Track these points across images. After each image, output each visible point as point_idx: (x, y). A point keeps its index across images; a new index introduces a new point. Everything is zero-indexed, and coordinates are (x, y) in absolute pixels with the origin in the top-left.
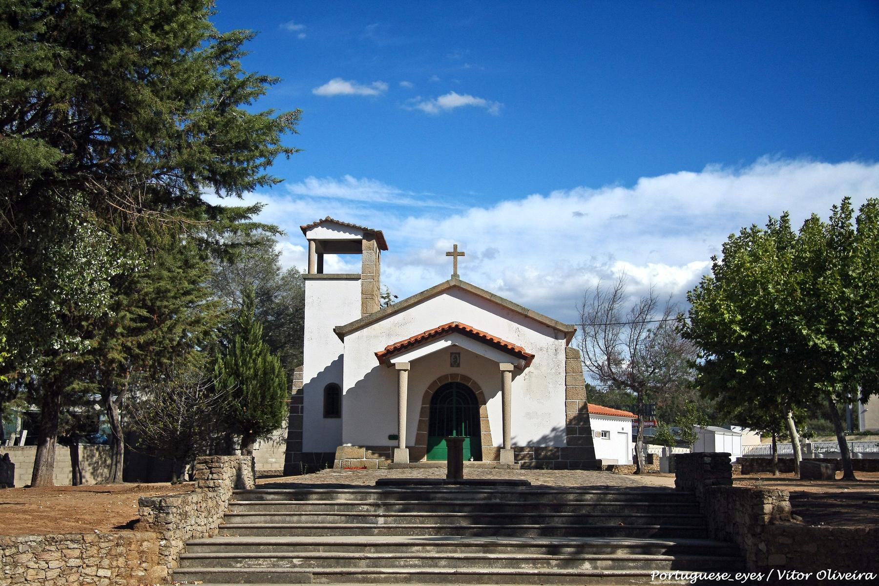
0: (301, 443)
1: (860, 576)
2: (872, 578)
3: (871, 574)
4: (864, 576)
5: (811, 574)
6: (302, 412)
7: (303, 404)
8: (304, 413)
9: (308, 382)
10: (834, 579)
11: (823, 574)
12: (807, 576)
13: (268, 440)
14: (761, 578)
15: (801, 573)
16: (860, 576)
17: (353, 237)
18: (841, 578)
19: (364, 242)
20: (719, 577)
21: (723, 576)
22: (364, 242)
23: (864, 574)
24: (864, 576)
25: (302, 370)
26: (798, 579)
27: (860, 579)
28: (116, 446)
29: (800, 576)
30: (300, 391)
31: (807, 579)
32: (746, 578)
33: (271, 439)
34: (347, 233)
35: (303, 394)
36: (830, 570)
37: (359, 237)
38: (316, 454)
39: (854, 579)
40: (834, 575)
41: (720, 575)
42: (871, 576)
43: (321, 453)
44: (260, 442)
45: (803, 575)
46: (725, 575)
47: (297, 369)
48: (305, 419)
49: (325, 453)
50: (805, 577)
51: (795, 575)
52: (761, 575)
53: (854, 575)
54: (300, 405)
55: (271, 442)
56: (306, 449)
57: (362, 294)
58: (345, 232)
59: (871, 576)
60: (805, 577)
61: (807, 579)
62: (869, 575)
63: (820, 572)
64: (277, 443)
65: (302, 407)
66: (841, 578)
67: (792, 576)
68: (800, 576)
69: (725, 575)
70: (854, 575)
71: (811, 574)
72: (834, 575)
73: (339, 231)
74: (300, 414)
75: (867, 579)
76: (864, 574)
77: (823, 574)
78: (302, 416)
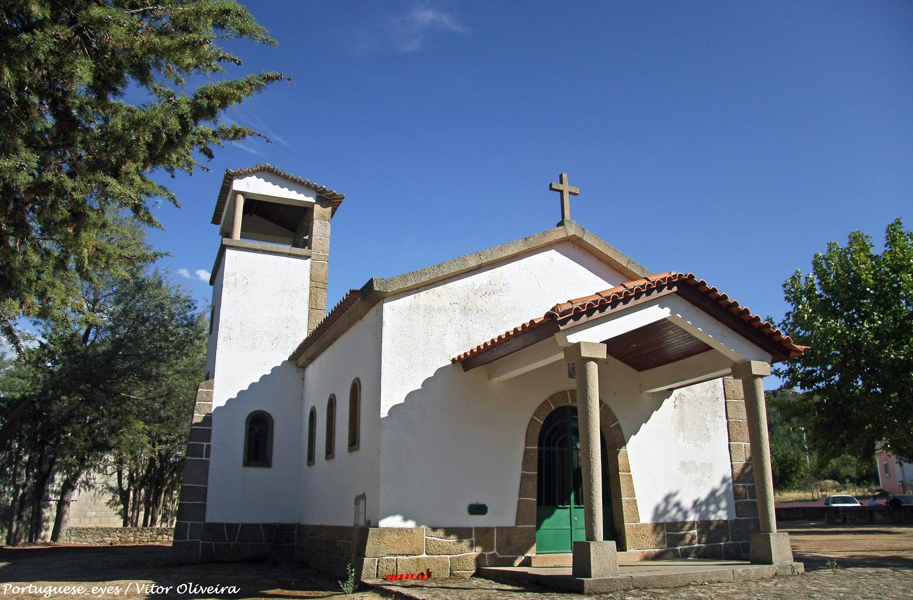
0: (204, 506)
1: (223, 590)
2: (235, 592)
3: (235, 588)
4: (227, 590)
5: (172, 587)
6: (208, 456)
7: (209, 441)
8: (211, 456)
9: (223, 404)
10: (195, 593)
11: (184, 587)
12: (167, 590)
13: (89, 488)
14: (118, 591)
15: (161, 587)
16: (223, 590)
17: (301, 197)
18: (203, 592)
19: (317, 208)
20: (75, 591)
21: (78, 590)
22: (317, 208)
23: (227, 587)
24: (227, 590)
25: (211, 387)
26: (158, 593)
27: (222, 593)
28: (522, 588)
29: (160, 590)
30: (208, 419)
31: (166, 593)
32: (103, 592)
33: (93, 487)
34: (286, 189)
35: (211, 426)
36: (191, 584)
37: (311, 199)
38: (230, 526)
39: (216, 593)
40: (195, 589)
41: (76, 589)
42: (234, 590)
43: (237, 525)
44: (80, 491)
45: (163, 589)
46: (81, 588)
47: (203, 383)
48: (211, 467)
49: (243, 525)
50: (165, 590)
51: (155, 589)
52: (119, 589)
53: (217, 589)
54: (205, 444)
55: (93, 491)
56: (212, 517)
57: (311, 280)
58: (290, 190)
59: (234, 590)
60: (165, 590)
61: (166, 593)
62: (232, 589)
63: (181, 586)
64: (100, 492)
65: (209, 447)
66: (203, 592)
67: (152, 590)
68: (160, 590)
69: (81, 588)
70: (217, 589)
71: (172, 587)
72: (195, 589)
73: (282, 187)
74: (204, 458)
75: (229, 592)
76: (227, 587)
77: (184, 587)
78: (208, 461)
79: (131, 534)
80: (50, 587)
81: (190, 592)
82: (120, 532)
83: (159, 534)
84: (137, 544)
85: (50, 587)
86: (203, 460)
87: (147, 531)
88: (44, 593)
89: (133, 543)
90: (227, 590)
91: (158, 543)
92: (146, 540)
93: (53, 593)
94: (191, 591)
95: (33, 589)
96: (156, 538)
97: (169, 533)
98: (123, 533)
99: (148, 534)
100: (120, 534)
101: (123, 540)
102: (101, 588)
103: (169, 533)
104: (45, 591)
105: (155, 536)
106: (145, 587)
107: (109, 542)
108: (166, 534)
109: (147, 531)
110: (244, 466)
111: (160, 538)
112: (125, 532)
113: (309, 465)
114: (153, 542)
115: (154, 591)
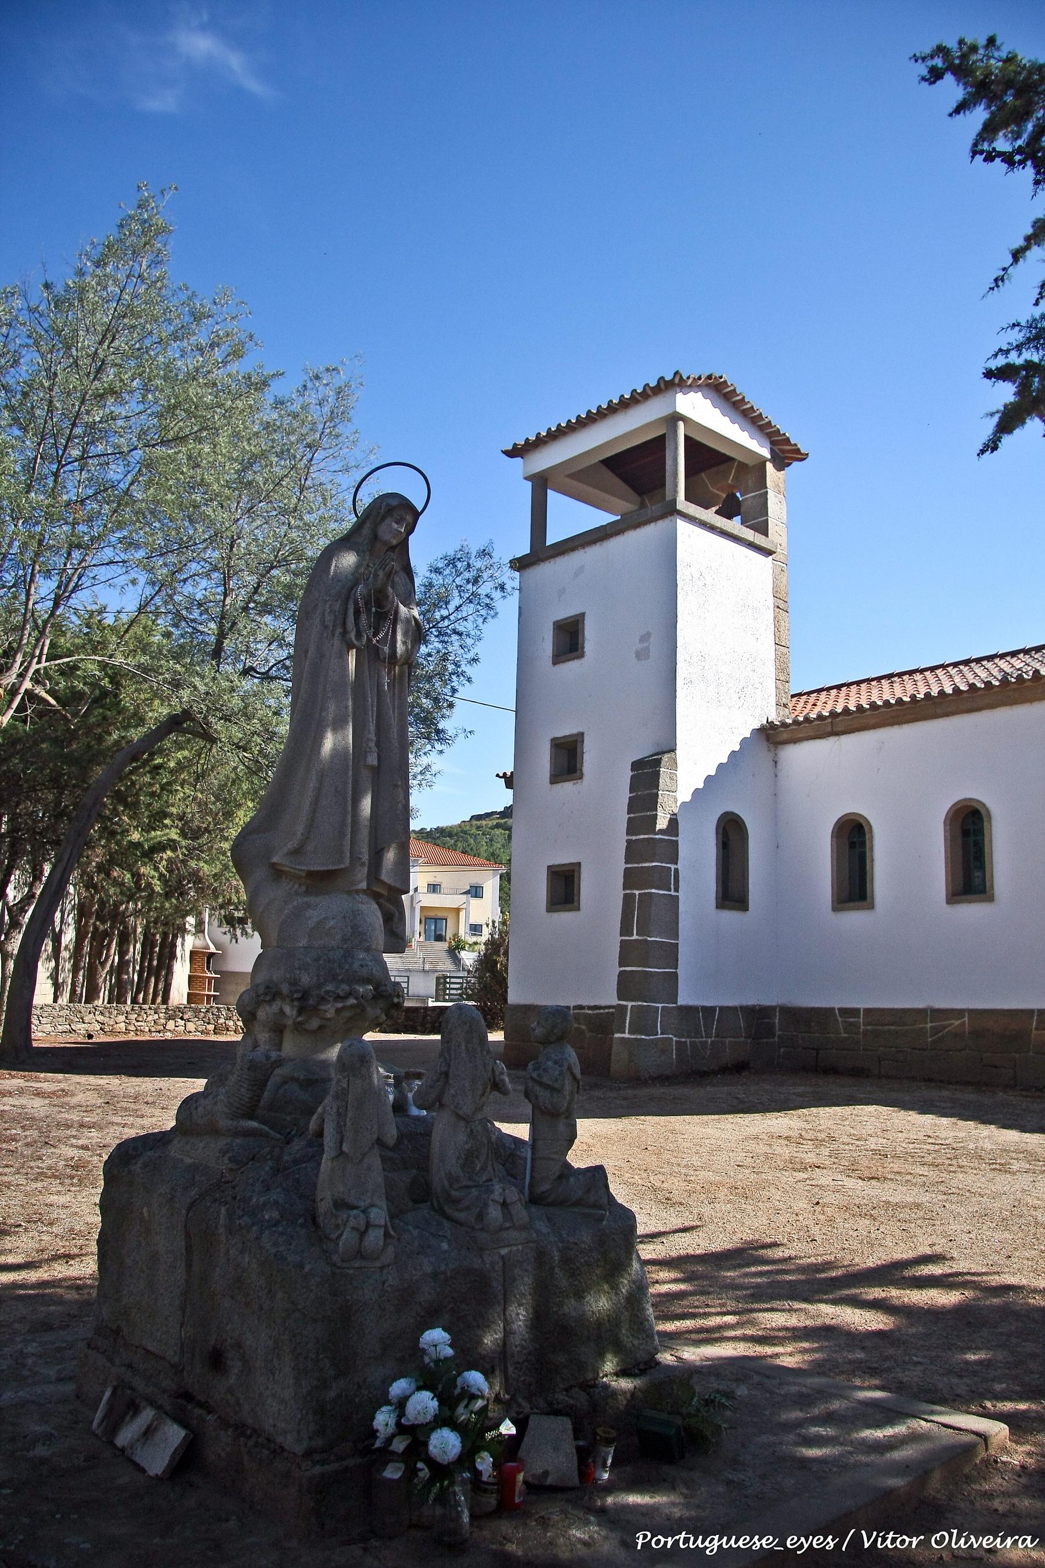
3: (1029, 1538)
5: (922, 1537)
12: (915, 1541)
14: (832, 1544)
15: (904, 1537)
18: (975, 1546)
20: (758, 1544)
21: (764, 1541)
23: (1017, 1537)
29: (903, 1542)
32: (806, 1546)
36: (955, 1531)
40: (963, 1540)
41: (759, 1540)
42: (1028, 1542)
52: (833, 1540)
53: (999, 1540)
59: (1028, 1542)
62: (1025, 1540)
63: (938, 1535)
66: (975, 1546)
67: (888, 1542)
68: (903, 1542)
70: (999, 1540)
71: (922, 1537)
72: (963, 1540)
74: (672, 893)
77: (943, 1537)
79: (122, 1018)
80: (717, 1537)
81: (954, 1546)
82: (102, 1014)
83: (169, 1018)
84: (132, 1037)
85: (717, 1537)
86: (638, 889)
87: (149, 1012)
88: (706, 1548)
89: (125, 1033)
90: (1016, 1541)
91: (169, 1036)
92: (147, 1029)
93: (720, 1546)
94: (956, 1544)
95: (686, 1540)
96: (164, 1026)
97: (186, 1017)
98: (107, 1014)
99: (150, 1018)
100: (100, 1018)
101: (107, 1029)
102: (803, 1539)
103: (186, 1017)
104: (707, 1543)
105: (163, 1021)
106: (877, 1536)
107: (83, 1032)
108: (182, 1018)
109: (149, 1012)
110: (717, 907)
111: (171, 1025)
112: (110, 1013)
113: (556, 778)
114: (159, 1032)
115: (892, 1544)
